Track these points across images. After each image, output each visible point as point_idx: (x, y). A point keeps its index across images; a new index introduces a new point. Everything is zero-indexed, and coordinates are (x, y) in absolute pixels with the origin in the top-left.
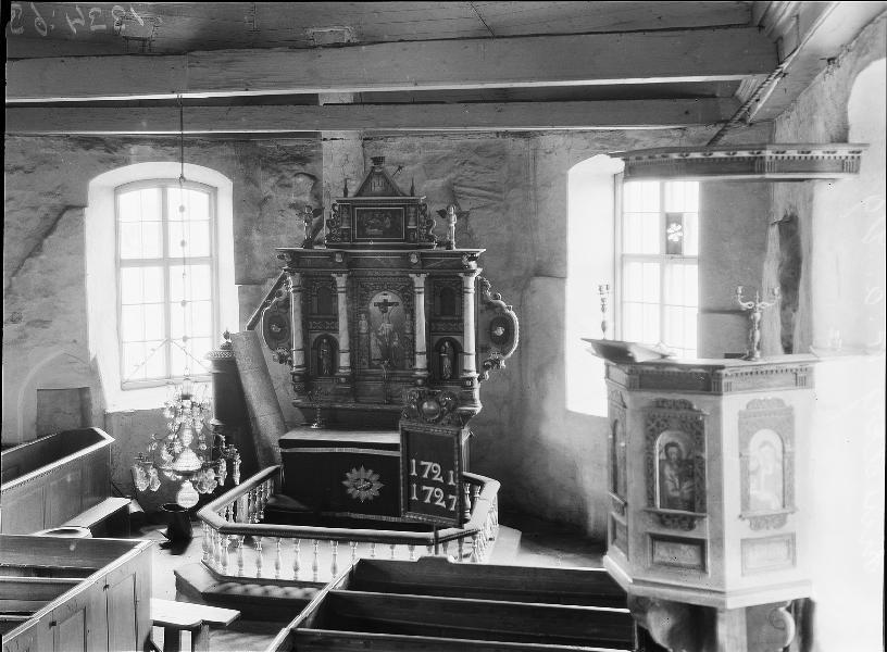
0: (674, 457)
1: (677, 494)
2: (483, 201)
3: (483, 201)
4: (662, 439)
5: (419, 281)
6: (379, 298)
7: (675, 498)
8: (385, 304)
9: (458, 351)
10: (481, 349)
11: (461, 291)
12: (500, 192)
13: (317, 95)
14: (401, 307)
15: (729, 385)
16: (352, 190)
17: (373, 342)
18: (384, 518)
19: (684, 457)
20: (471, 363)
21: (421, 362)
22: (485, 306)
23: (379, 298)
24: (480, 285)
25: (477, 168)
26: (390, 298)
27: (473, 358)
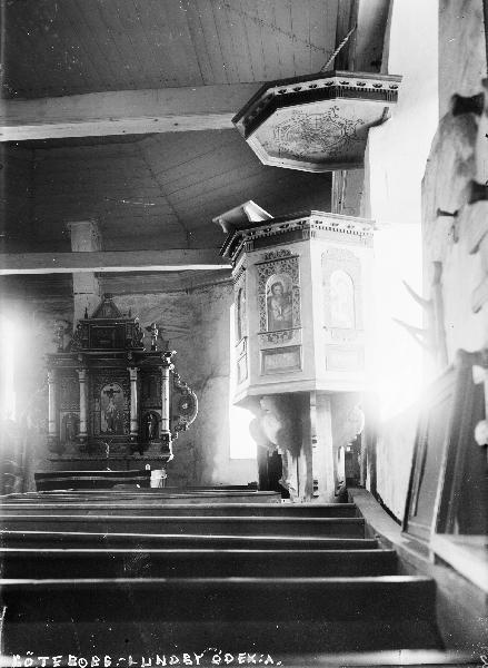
0: (278, 292)
1: (280, 318)
2: (177, 334)
3: (177, 334)
4: (271, 281)
5: (133, 373)
6: (108, 388)
7: (279, 322)
8: (110, 393)
9: (158, 420)
10: (173, 418)
11: (161, 377)
12: (188, 328)
13: (71, 274)
14: (122, 394)
15: (314, 234)
16: (90, 313)
17: (103, 417)
18: (104, 478)
19: (285, 291)
20: (166, 425)
21: (133, 426)
22: (175, 389)
23: (108, 388)
24: (174, 376)
25: (174, 314)
26: (115, 387)
27: (168, 422)
